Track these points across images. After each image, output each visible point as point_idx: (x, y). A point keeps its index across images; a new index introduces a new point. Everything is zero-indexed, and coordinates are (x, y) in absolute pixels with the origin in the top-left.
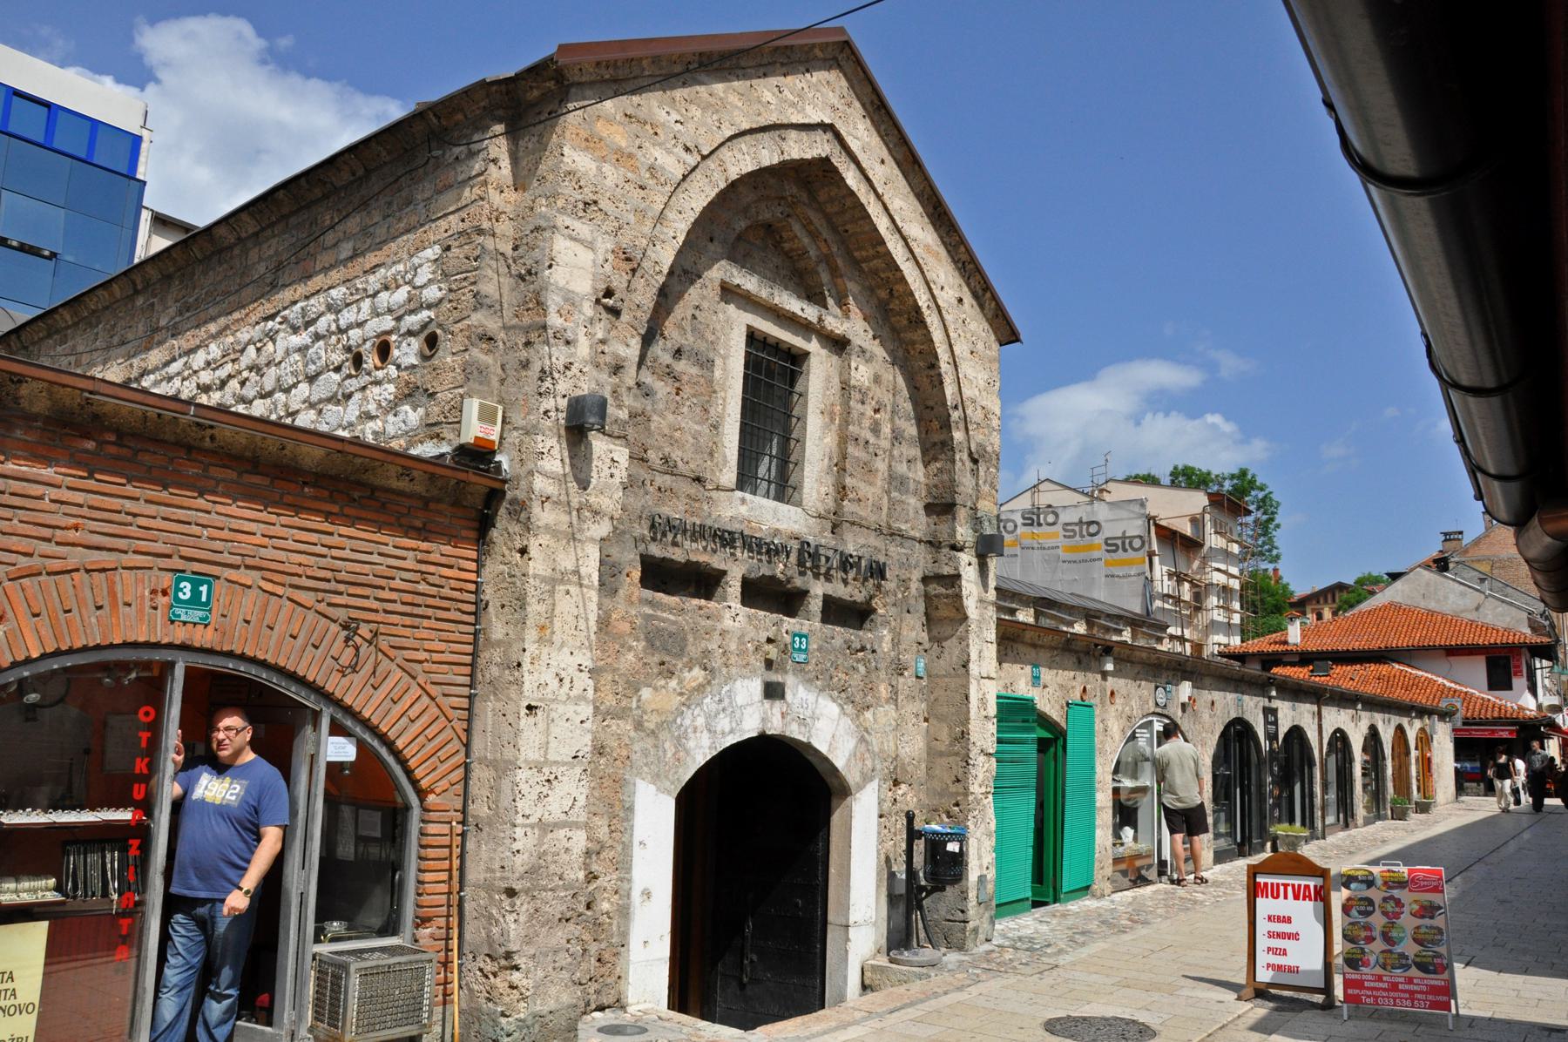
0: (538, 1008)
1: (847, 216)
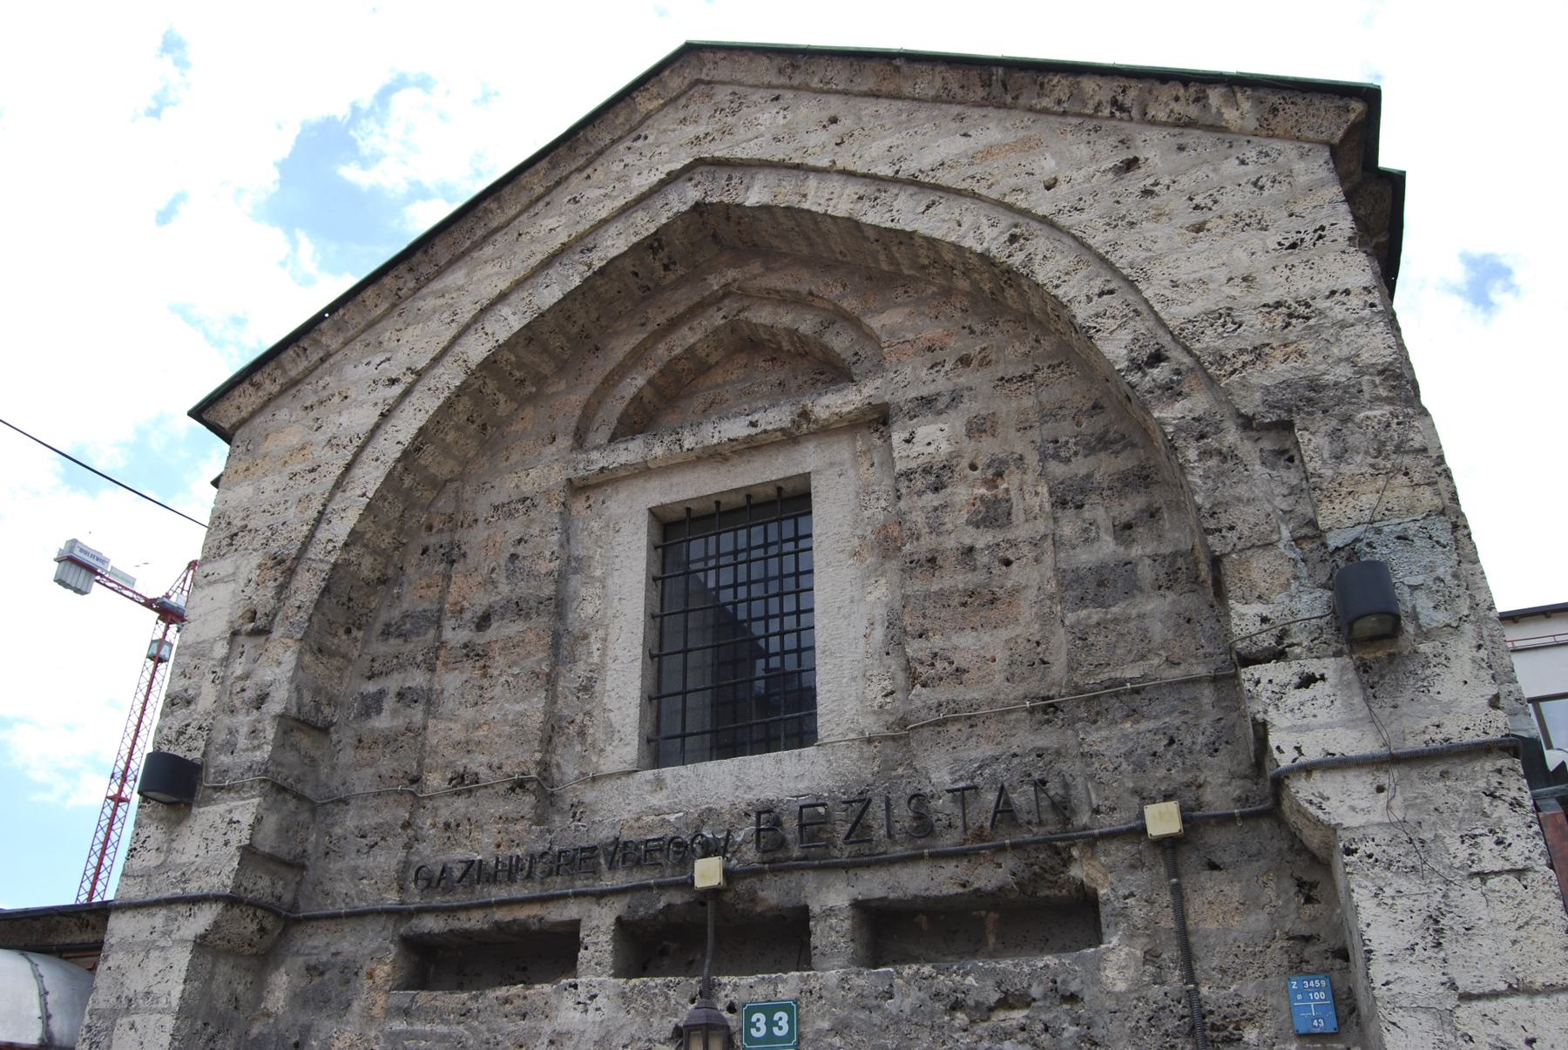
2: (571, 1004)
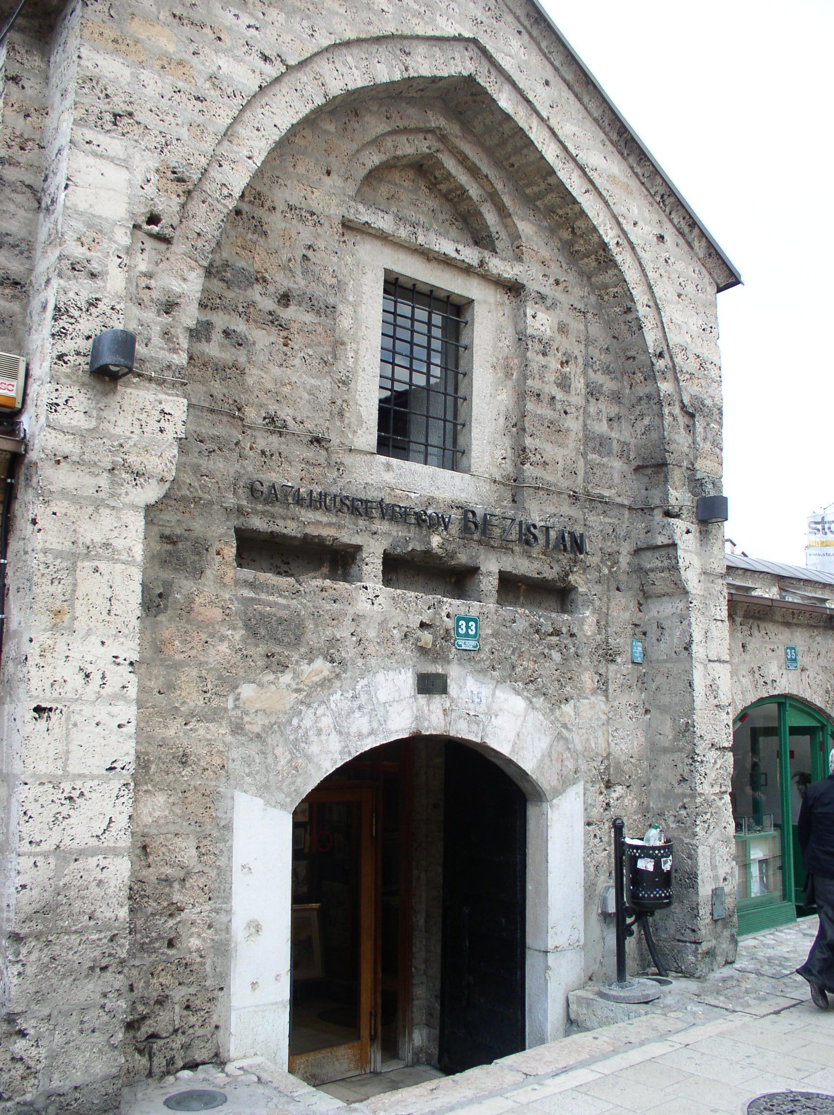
0: (55, 1084)
1: (509, 147)
2: (364, 598)
